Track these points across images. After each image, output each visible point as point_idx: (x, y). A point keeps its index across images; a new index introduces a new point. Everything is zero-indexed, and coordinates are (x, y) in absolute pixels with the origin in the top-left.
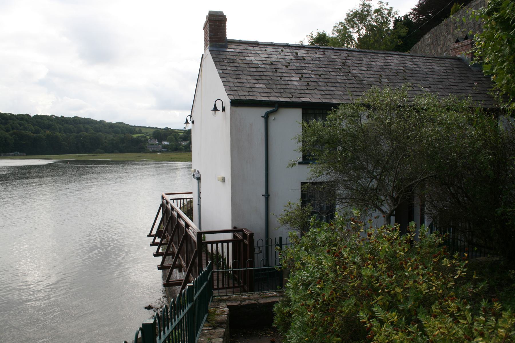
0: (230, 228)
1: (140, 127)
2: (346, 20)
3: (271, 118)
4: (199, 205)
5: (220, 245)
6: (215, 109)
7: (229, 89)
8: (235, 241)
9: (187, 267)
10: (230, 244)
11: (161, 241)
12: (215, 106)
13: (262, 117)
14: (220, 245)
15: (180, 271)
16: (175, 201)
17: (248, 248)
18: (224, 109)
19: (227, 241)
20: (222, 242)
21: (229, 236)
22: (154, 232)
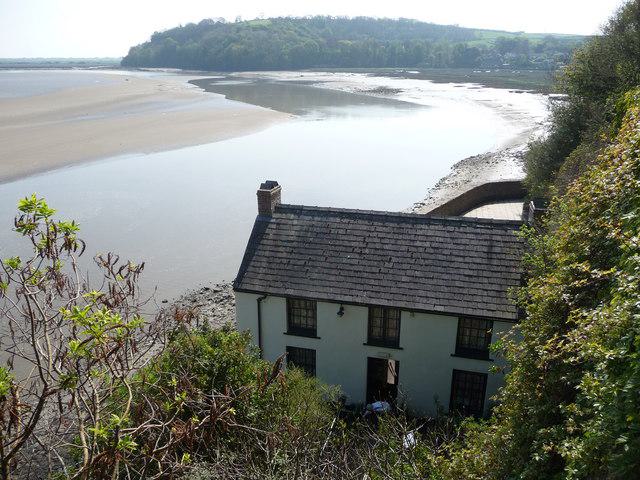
13: (268, 194)
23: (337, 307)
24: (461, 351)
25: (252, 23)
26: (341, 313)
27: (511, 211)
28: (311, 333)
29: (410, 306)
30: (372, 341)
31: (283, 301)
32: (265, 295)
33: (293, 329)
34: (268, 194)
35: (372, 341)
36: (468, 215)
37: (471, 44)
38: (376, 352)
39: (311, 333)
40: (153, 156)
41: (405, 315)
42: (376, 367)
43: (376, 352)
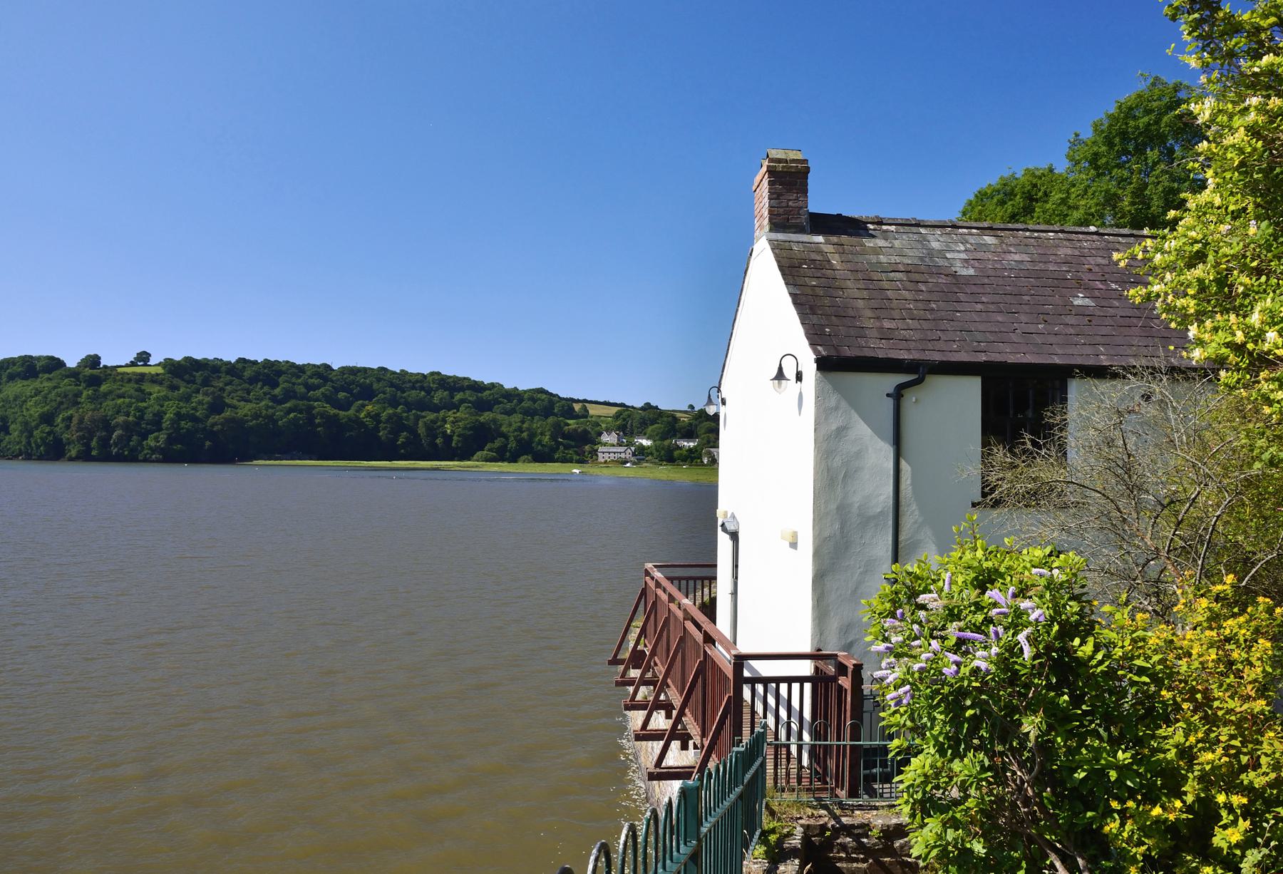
0: (807, 649)
1: (585, 401)
2: (105, 367)
3: (910, 397)
4: (735, 593)
5: (796, 686)
6: (780, 376)
7: (815, 336)
8: (819, 681)
9: (703, 735)
10: (808, 686)
11: (643, 675)
12: (780, 369)
13: (888, 395)
14: (796, 686)
15: (684, 747)
16: (676, 582)
17: (849, 699)
18: (799, 377)
19: (801, 680)
20: (790, 680)
21: (806, 668)
22: (626, 655)
25: (120, 370)
34: (888, 395)
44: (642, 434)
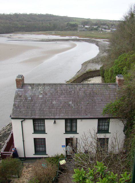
3: (23, 122)
13: (20, 82)
23: (53, 121)
24: (100, 131)
26: (55, 122)
27: (97, 80)
28: (43, 132)
29: (80, 117)
30: (67, 132)
31: (31, 121)
32: (25, 119)
33: (36, 131)
34: (20, 82)
35: (67, 132)
36: (86, 82)
37: (72, 23)
38: (102, 136)
39: (43, 132)
40: (69, 50)
41: (78, 121)
42: (69, 141)
43: (102, 136)
44: (86, 25)
